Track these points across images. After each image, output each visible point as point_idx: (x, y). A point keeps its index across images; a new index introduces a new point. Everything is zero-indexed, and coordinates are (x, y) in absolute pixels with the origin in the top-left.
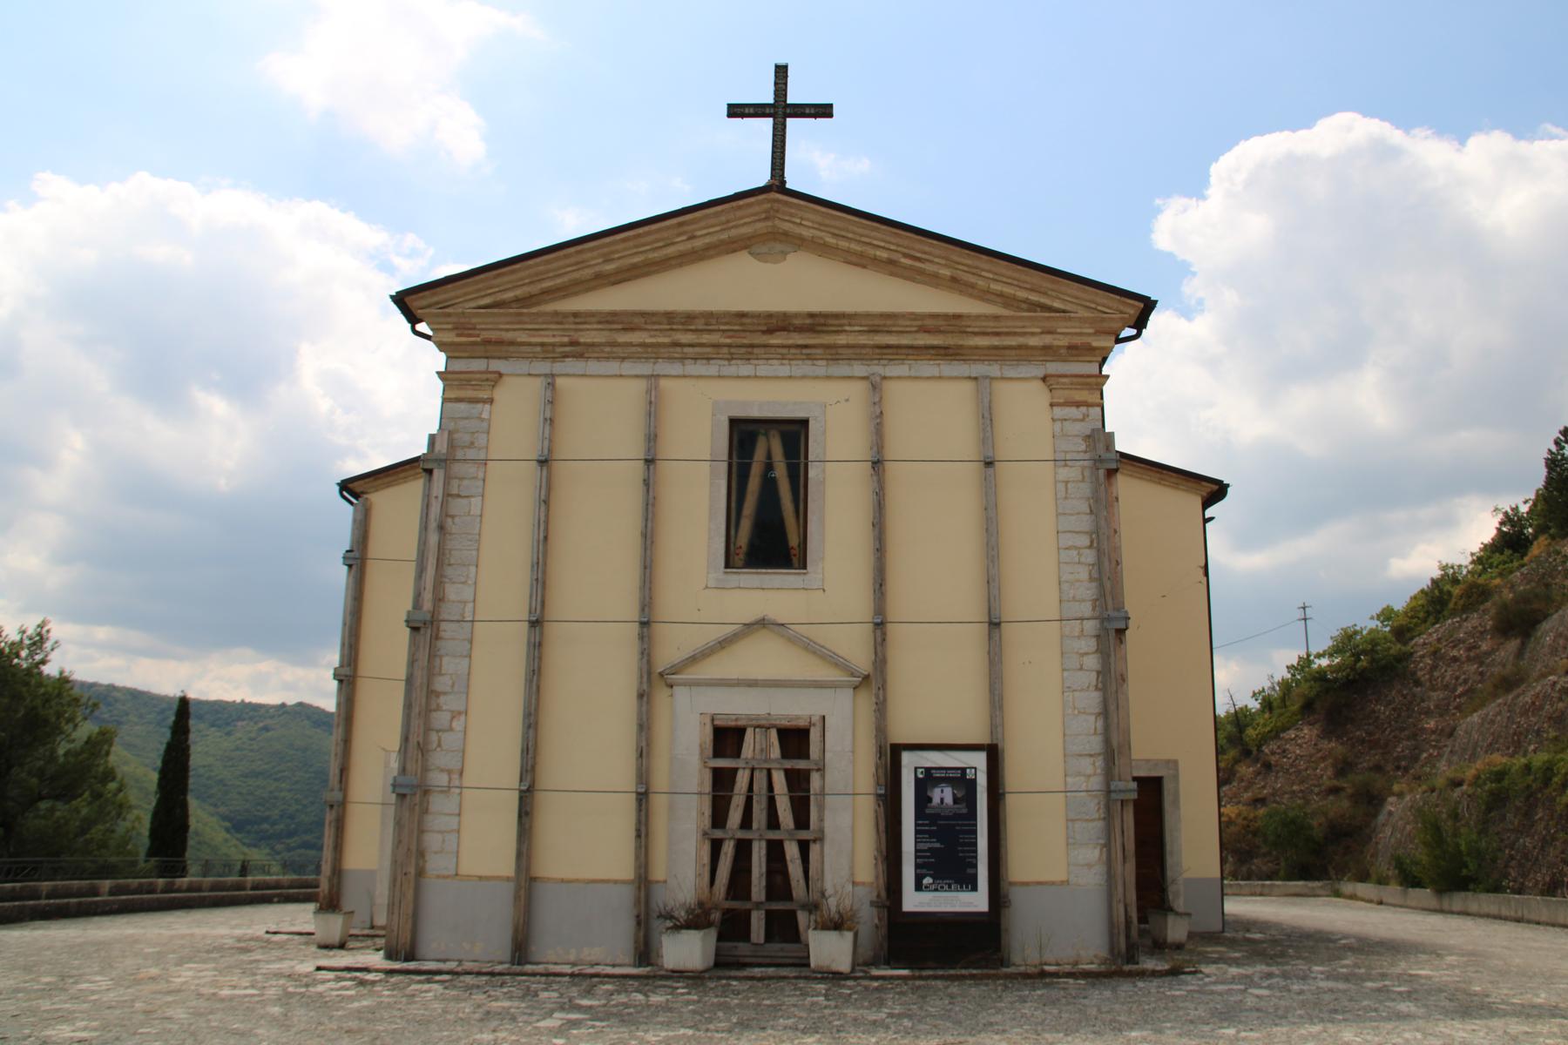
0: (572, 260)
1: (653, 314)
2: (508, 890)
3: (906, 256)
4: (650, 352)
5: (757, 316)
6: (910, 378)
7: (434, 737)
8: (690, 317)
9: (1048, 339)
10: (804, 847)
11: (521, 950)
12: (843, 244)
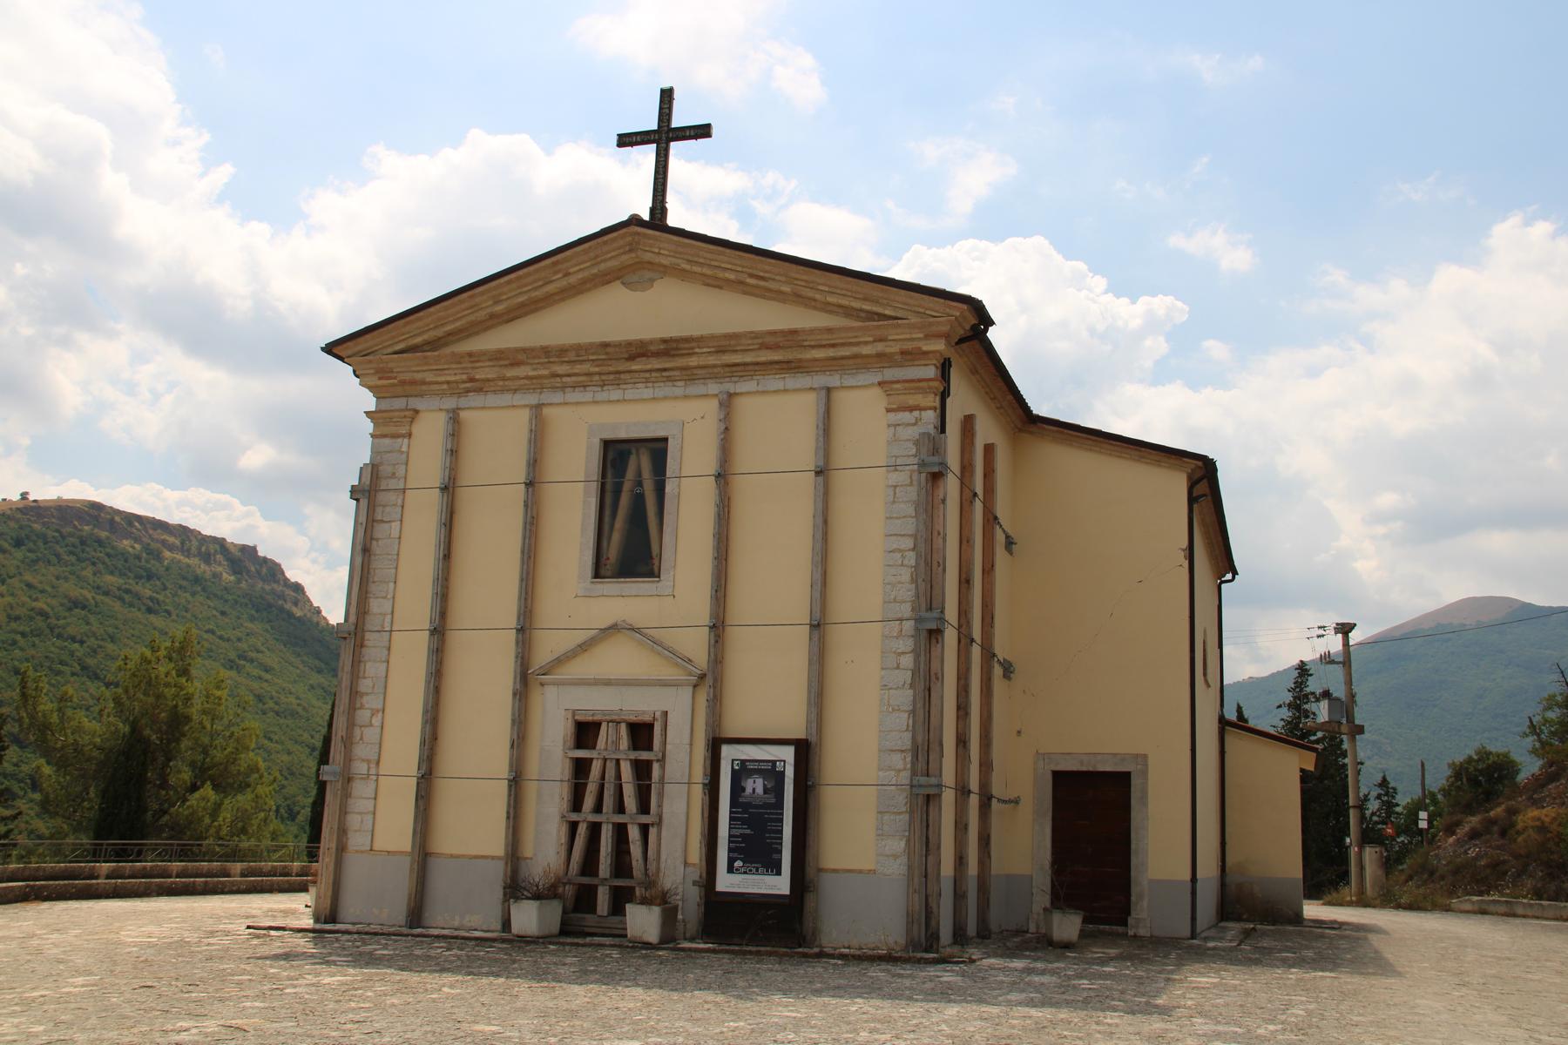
0: (466, 305)
1: (532, 350)
2: (406, 862)
3: (751, 276)
4: (535, 384)
5: (618, 345)
6: (757, 392)
7: (357, 731)
8: (562, 351)
9: (880, 347)
10: (645, 829)
11: (416, 916)
12: (696, 269)
